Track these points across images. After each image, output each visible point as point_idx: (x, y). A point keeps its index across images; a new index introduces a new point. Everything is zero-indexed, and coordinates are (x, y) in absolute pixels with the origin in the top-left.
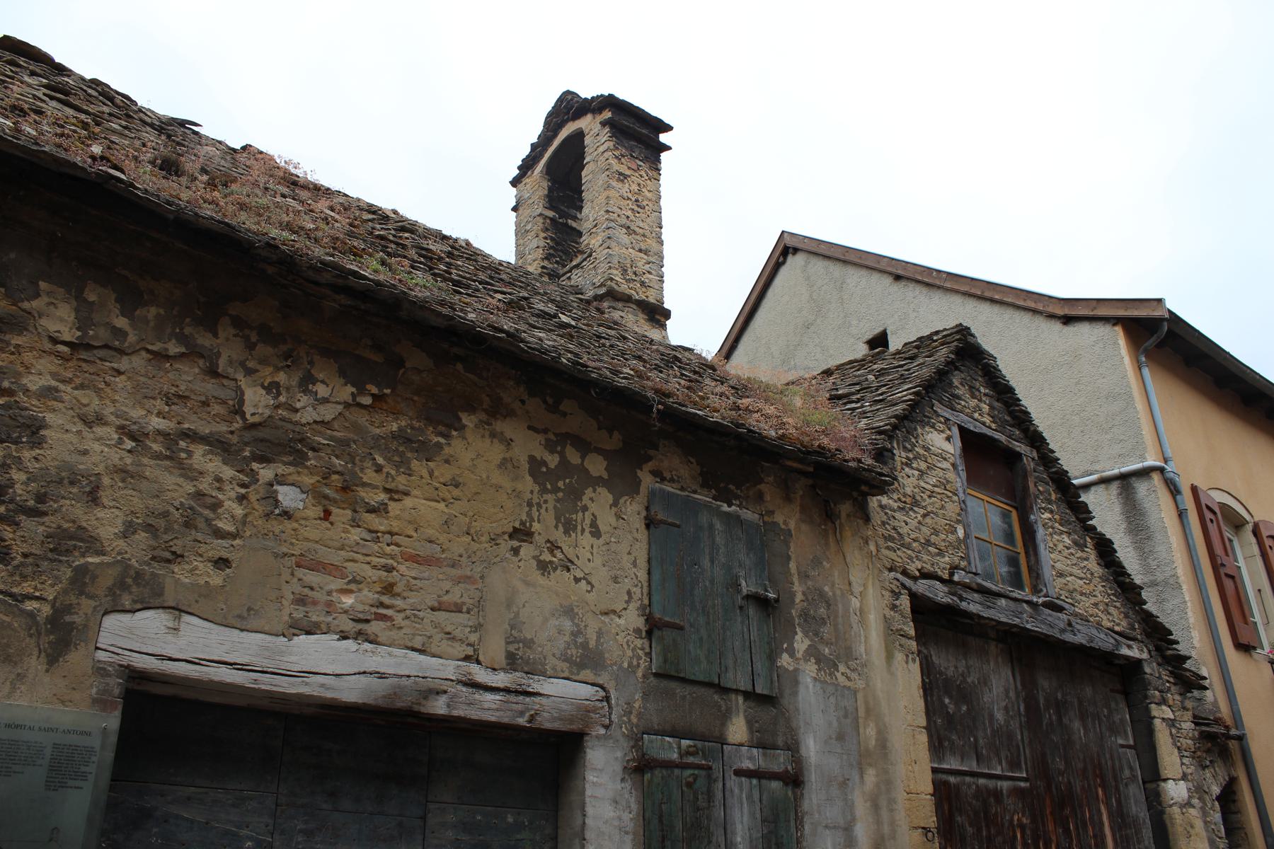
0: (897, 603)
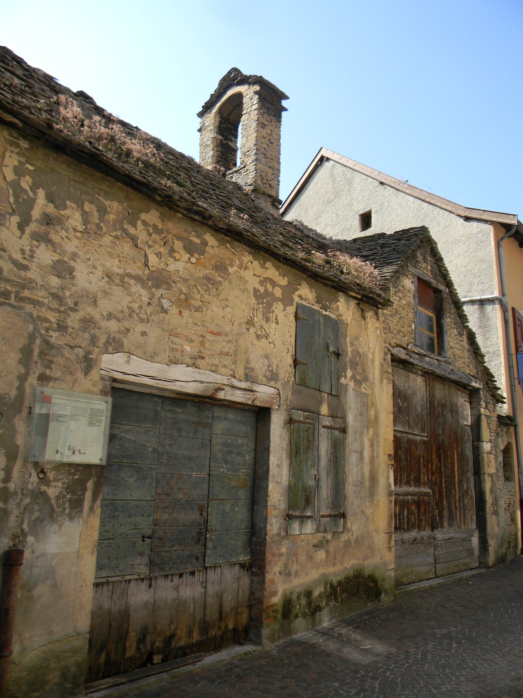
0: (386, 357)
